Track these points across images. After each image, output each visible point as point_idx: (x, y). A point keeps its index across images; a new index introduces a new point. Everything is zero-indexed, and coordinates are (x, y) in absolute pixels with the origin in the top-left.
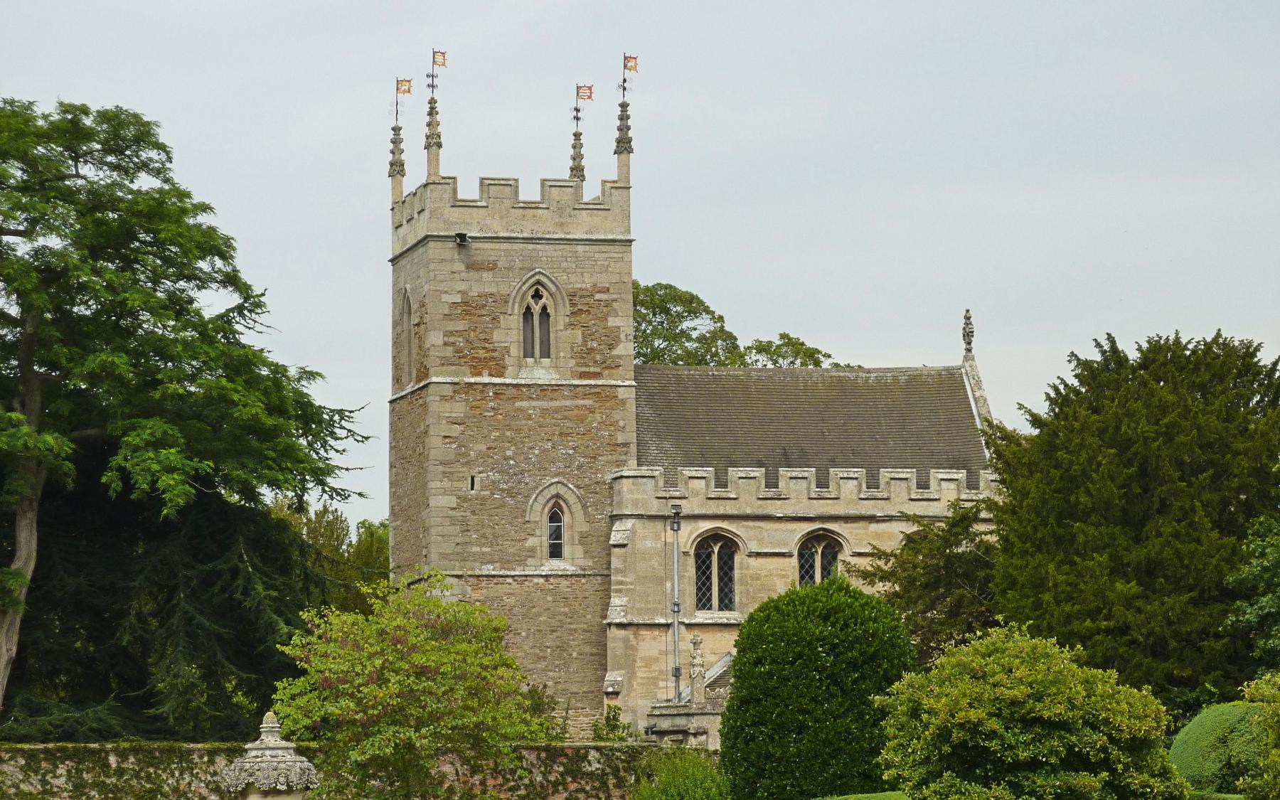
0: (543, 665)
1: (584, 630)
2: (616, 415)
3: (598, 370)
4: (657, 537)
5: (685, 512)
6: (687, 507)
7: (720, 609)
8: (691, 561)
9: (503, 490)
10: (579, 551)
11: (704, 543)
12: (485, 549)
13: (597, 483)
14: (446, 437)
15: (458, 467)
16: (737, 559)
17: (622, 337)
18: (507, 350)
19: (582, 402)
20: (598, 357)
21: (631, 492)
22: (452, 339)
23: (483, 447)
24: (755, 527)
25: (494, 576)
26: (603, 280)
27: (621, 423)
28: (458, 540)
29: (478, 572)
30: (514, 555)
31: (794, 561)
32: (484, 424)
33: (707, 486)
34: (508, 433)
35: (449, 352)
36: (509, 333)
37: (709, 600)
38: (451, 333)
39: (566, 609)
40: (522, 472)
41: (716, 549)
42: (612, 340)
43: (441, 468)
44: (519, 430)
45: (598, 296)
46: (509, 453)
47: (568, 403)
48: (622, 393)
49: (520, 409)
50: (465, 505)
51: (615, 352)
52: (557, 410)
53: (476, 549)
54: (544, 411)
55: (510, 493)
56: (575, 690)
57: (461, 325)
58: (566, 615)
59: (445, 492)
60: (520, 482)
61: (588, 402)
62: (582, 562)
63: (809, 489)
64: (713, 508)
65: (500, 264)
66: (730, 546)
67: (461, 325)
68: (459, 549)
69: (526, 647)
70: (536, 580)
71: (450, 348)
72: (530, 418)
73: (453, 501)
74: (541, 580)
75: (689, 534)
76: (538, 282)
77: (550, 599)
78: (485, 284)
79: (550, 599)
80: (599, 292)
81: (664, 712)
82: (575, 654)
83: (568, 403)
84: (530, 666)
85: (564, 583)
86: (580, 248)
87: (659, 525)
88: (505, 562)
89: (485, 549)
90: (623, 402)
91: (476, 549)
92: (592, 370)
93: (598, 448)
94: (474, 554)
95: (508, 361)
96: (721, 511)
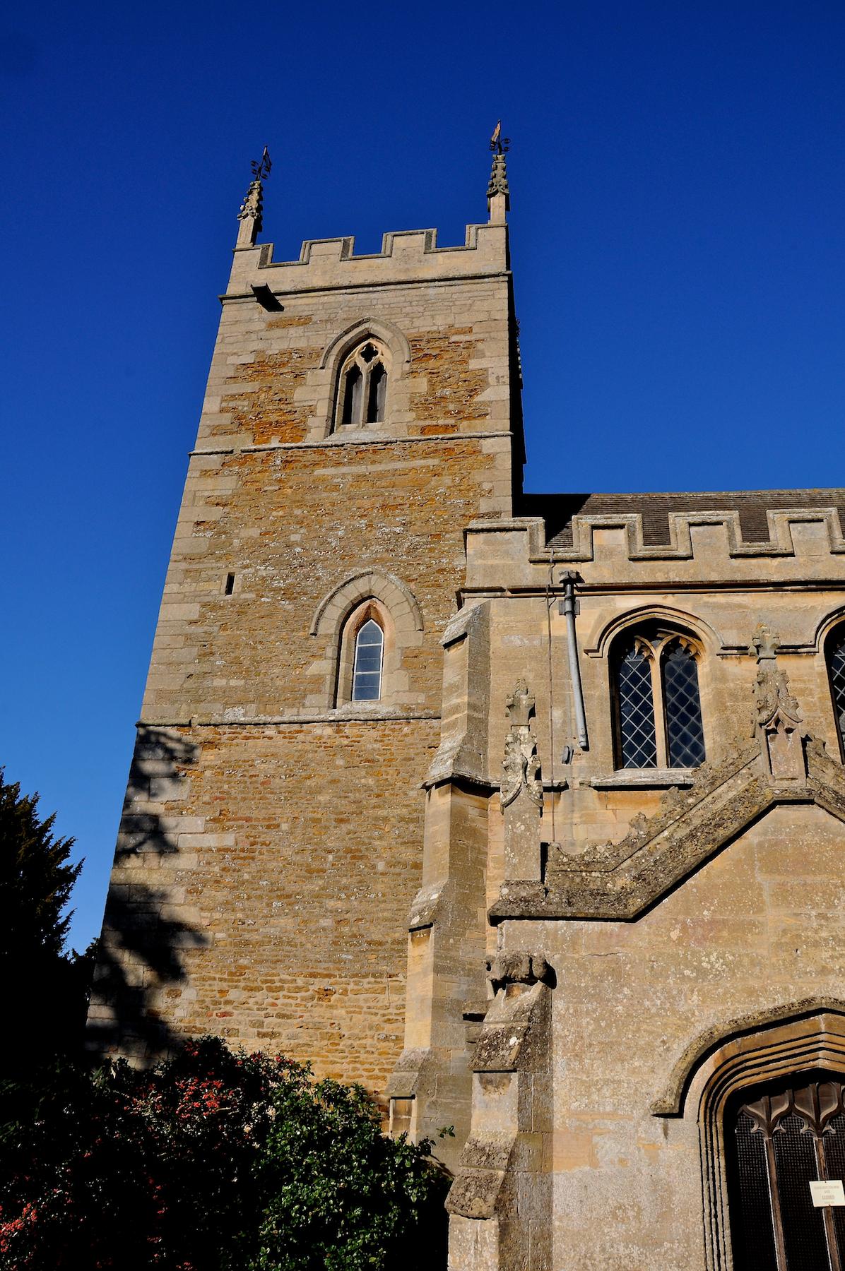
0: (316, 884)
1: (402, 819)
2: (477, 476)
3: (451, 422)
4: (533, 628)
5: (588, 581)
6: (589, 574)
7: (671, 763)
8: (602, 668)
9: (278, 590)
10: (403, 678)
11: (625, 641)
12: (233, 683)
13: (441, 571)
14: (198, 524)
15: (210, 563)
16: (703, 668)
17: (492, 380)
18: (312, 412)
19: (422, 462)
20: (451, 407)
21: (482, 555)
22: (232, 404)
23: (254, 532)
24: (728, 606)
25: (242, 725)
26: (464, 320)
27: (486, 486)
28: (191, 670)
29: (216, 719)
30: (284, 689)
31: (819, 662)
32: (262, 502)
33: (631, 538)
34: (298, 512)
35: (227, 419)
36: (316, 392)
37: (650, 749)
38: (233, 397)
39: (371, 781)
40: (313, 563)
41: (657, 653)
42: (476, 384)
43: (184, 566)
44: (315, 507)
45: (454, 338)
46: (295, 538)
47: (399, 465)
48: (487, 446)
49: (323, 479)
50: (212, 615)
51: (477, 399)
52: (380, 475)
53: (219, 682)
54: (359, 478)
55: (289, 594)
56: (376, 937)
57: (248, 387)
58: (368, 789)
59: (184, 599)
60: (307, 577)
61: (431, 462)
62: (406, 699)
63: (831, 539)
64: (643, 573)
65: (314, 319)
66: (680, 645)
67: (248, 387)
68: (190, 684)
69: (287, 852)
70: (318, 730)
71: (229, 415)
72: (335, 488)
73: (193, 611)
74: (328, 731)
75: (595, 615)
76: (370, 336)
77: (340, 762)
78: (296, 339)
79: (340, 762)
80: (457, 333)
81: (781, 1055)
82: (381, 866)
83: (399, 465)
84: (291, 888)
85: (371, 734)
86: (432, 291)
87: (535, 604)
88: (263, 700)
89: (233, 683)
90: (491, 458)
91: (219, 682)
92: (441, 422)
93: (446, 522)
94: (215, 690)
95: (311, 421)
96: (660, 578)
